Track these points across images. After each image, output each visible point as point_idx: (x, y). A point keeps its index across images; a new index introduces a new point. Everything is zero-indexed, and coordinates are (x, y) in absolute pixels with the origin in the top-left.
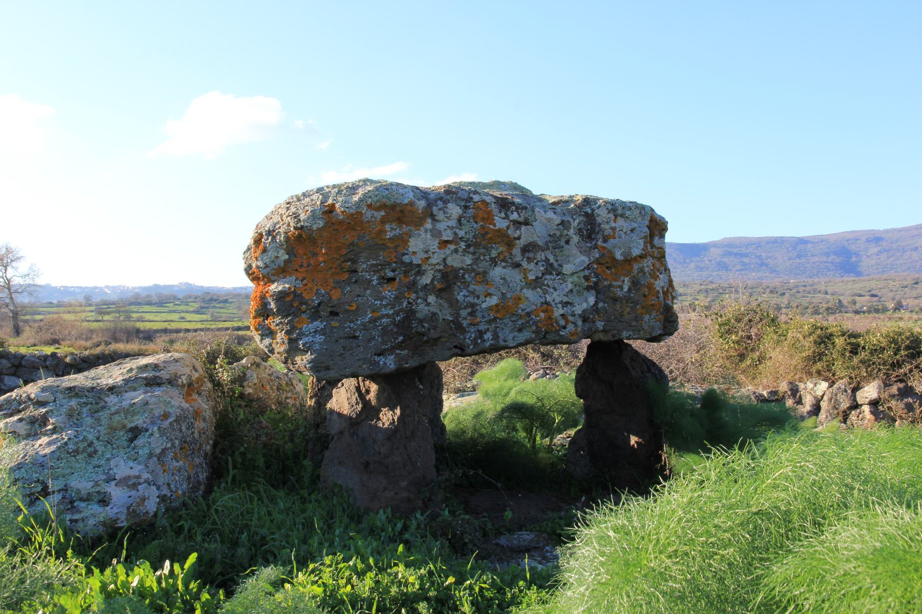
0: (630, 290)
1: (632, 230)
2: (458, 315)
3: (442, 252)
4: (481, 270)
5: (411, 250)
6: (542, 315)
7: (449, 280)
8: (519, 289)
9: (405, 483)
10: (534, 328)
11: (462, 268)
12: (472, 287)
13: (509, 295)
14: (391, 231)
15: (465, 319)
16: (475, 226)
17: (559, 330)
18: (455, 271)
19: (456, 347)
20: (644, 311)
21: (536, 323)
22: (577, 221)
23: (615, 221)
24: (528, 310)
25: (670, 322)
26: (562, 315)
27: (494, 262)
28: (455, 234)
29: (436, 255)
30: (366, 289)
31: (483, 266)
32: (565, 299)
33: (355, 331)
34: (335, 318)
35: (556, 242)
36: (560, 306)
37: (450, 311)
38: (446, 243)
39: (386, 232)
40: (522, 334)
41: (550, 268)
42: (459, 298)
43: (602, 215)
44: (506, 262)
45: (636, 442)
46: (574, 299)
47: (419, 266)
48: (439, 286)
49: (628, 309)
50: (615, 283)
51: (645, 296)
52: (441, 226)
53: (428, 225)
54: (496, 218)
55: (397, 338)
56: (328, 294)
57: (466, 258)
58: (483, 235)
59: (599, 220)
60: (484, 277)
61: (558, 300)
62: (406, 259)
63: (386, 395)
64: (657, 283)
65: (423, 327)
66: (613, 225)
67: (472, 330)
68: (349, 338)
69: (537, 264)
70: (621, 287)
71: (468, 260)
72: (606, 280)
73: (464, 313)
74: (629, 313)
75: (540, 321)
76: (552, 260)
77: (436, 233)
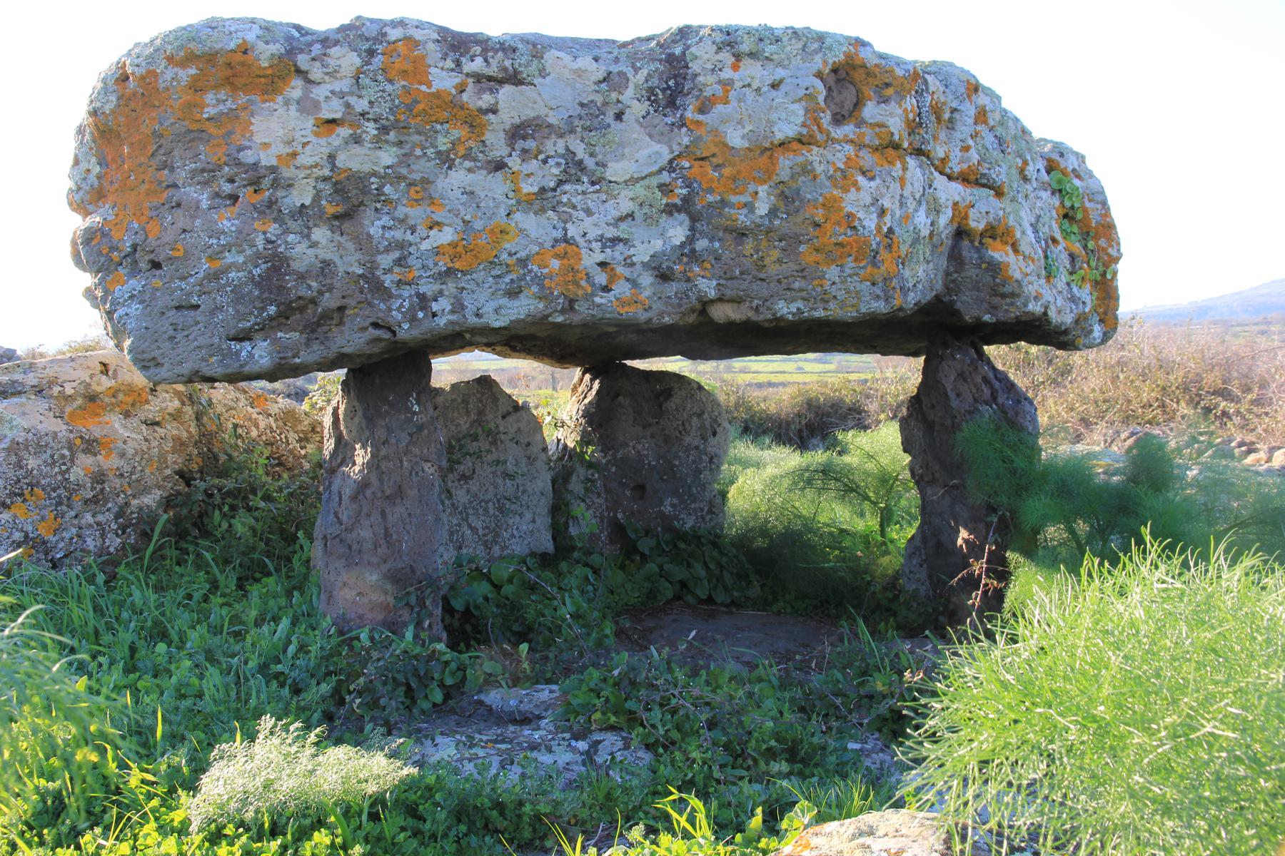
0: (773, 212)
1: (775, 86)
2: (373, 266)
3: (323, 141)
4: (417, 176)
5: (258, 139)
6: (555, 264)
7: (348, 200)
8: (503, 212)
9: (374, 578)
10: (535, 289)
11: (374, 174)
12: (401, 211)
13: (478, 225)
14: (213, 104)
16: (389, 88)
17: (593, 295)
18: (360, 180)
19: (376, 325)
20: (821, 257)
21: (539, 280)
22: (645, 72)
23: (735, 68)
24: (522, 254)
26: (602, 265)
27: (446, 161)
28: (348, 106)
29: (308, 148)
30: (194, 217)
31: (421, 168)
32: (611, 232)
33: (190, 294)
34: (158, 272)
35: (594, 118)
36: (596, 246)
37: (358, 255)
39: (203, 106)
40: (516, 303)
41: (574, 169)
42: (372, 231)
43: (702, 56)
44: (475, 160)
45: (966, 541)
46: (636, 231)
47: (273, 169)
48: (331, 210)
50: (734, 199)
51: (817, 225)
52: (319, 93)
53: (295, 89)
54: (432, 70)
55: (263, 309)
56: (143, 229)
57: (381, 154)
58: (410, 108)
59: (695, 67)
60: (425, 190)
62: (248, 157)
63: (357, 420)
64: (852, 195)
65: (309, 287)
66: (727, 74)
67: (406, 294)
68: (178, 308)
69: (545, 162)
70: (750, 207)
71: (387, 157)
72: (711, 190)
73: (385, 260)
74: (779, 261)
76: (581, 154)
77: (307, 106)
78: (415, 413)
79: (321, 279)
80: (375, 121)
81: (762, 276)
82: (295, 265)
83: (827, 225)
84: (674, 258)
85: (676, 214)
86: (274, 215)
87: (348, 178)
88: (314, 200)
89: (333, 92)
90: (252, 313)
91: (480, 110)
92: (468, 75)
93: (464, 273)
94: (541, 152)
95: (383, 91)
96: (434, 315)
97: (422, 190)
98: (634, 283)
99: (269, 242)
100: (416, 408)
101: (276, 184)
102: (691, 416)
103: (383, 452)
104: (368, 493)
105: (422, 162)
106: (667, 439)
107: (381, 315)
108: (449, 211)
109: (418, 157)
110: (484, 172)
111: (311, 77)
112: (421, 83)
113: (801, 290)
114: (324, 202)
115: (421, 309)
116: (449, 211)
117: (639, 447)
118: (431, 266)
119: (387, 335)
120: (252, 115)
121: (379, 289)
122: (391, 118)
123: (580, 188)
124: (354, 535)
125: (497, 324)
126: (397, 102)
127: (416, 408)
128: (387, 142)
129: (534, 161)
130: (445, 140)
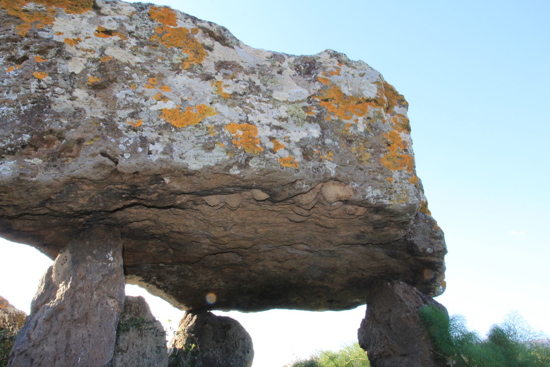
10: (225, 143)
11: (128, 65)
15: (124, 120)
16: (150, 23)
17: (264, 153)
18: (117, 65)
19: (104, 154)
20: (390, 163)
25: (436, 238)
27: (176, 69)
29: (88, 41)
31: (158, 69)
32: (276, 123)
38: (108, 33)
41: (253, 88)
46: (290, 126)
47: (60, 44)
49: (368, 156)
55: (20, 135)
61: (264, 121)
63: (66, 265)
65: (61, 124)
70: (356, 127)
72: (333, 114)
75: (237, 138)
76: (258, 83)
78: (110, 262)
79: (72, 118)
80: (137, 38)
81: (362, 167)
82: (54, 108)
83: (395, 145)
84: (314, 144)
85: (313, 123)
86: (50, 71)
87: (110, 62)
88: (82, 72)
89: (114, 19)
90: (8, 137)
91: (203, 45)
92: (199, 27)
93: (177, 130)
94: (235, 77)
95: (146, 24)
96: (150, 153)
97: (158, 79)
98: (291, 152)
99: (40, 87)
100: (111, 259)
101: (59, 53)
102: (239, 339)
103: (80, 285)
104: (61, 316)
105: (161, 66)
106: (227, 351)
107: (110, 145)
108: (174, 93)
109: (159, 63)
110: (199, 79)
111: (102, 11)
112: (171, 25)
113: (381, 181)
114: (89, 75)
115: (141, 146)
116: (174, 93)
117: (214, 352)
118: (155, 120)
119: (109, 162)
120: (57, 16)
121: (113, 130)
122: (148, 38)
123: (257, 97)
124: (39, 349)
125: (194, 165)
126: (153, 31)
127: (111, 259)
128: (141, 52)
129: (231, 81)
130: (178, 58)
